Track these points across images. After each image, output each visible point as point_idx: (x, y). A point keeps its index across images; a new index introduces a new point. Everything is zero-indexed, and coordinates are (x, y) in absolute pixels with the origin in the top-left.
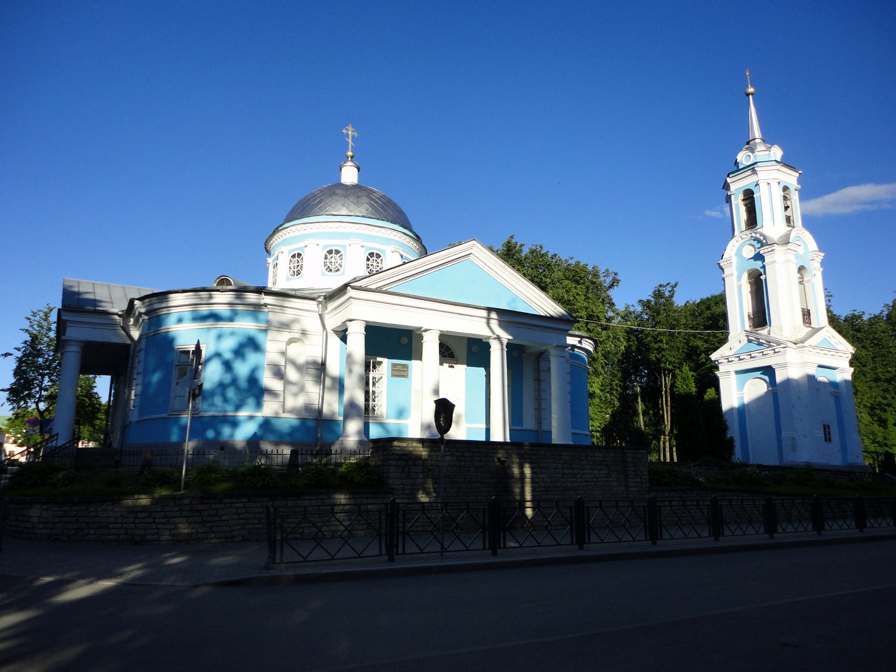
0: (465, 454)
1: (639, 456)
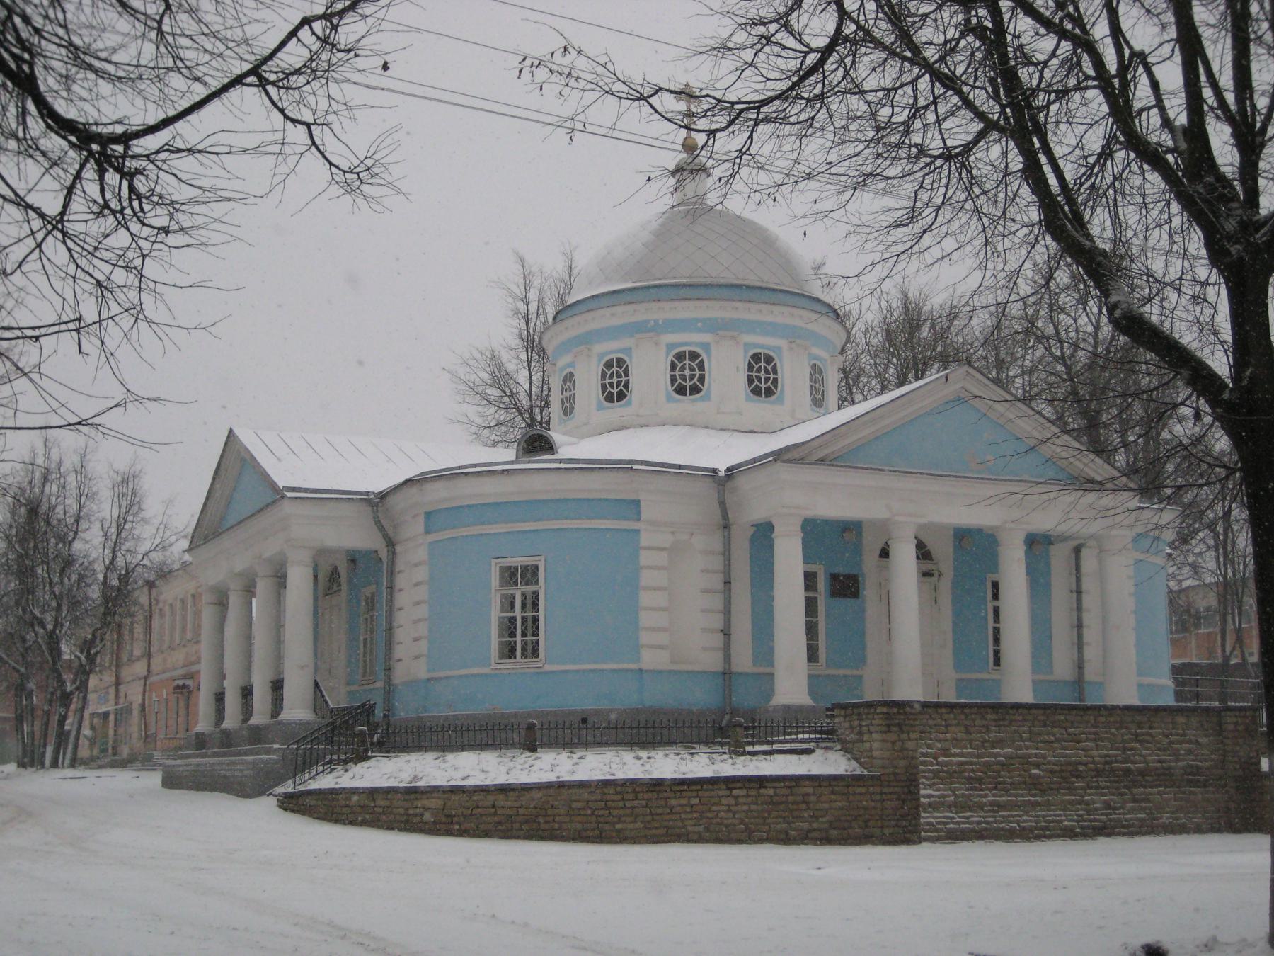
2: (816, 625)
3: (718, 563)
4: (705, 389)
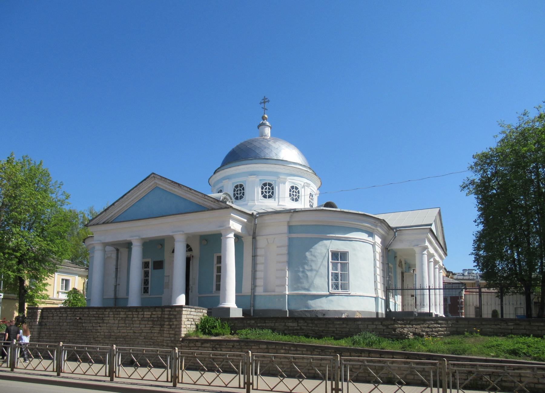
1: (175, 313)
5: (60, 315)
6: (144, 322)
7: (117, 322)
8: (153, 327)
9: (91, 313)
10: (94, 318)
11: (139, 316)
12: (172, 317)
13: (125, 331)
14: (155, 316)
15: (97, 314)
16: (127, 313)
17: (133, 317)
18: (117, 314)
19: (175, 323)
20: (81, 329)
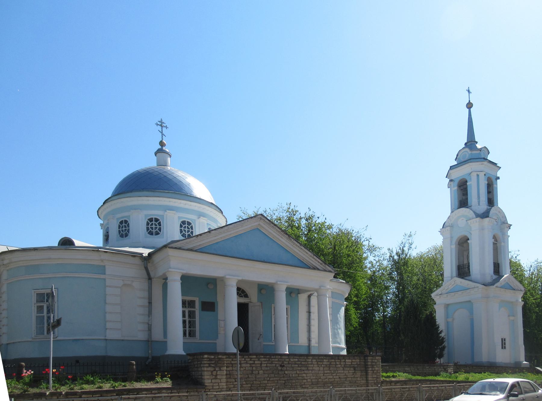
0: (256, 362)
1: (376, 361)
2: (195, 322)
3: (146, 294)
4: (161, 233)
5: (251, 362)
6: (347, 369)
7: (321, 369)
8: (355, 372)
9: (292, 360)
10: (297, 366)
11: (342, 363)
12: (374, 364)
13: (332, 377)
14: (355, 363)
15: (298, 361)
16: (330, 361)
17: (336, 364)
18: (321, 362)
19: (376, 369)
20: (284, 377)
